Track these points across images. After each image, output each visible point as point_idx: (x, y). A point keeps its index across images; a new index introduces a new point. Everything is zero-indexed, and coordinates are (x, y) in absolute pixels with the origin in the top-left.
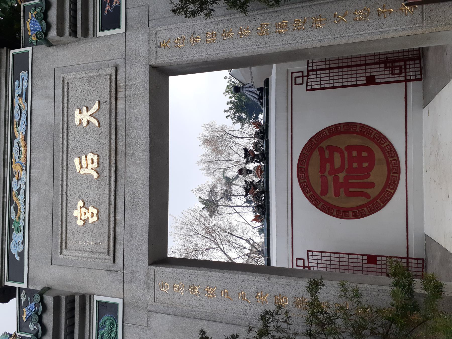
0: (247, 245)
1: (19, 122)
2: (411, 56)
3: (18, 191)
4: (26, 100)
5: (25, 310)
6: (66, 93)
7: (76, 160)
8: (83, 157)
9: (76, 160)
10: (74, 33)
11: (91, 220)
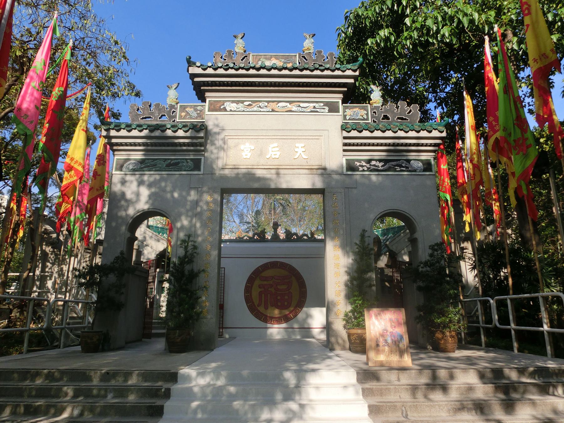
0: (469, 402)
1: (299, 106)
2: (180, 133)
3: (260, 107)
4: (312, 111)
5: (192, 109)
6: (314, 137)
7: (276, 145)
8: (278, 149)
9: (276, 145)
10: (345, 145)
11: (244, 154)
